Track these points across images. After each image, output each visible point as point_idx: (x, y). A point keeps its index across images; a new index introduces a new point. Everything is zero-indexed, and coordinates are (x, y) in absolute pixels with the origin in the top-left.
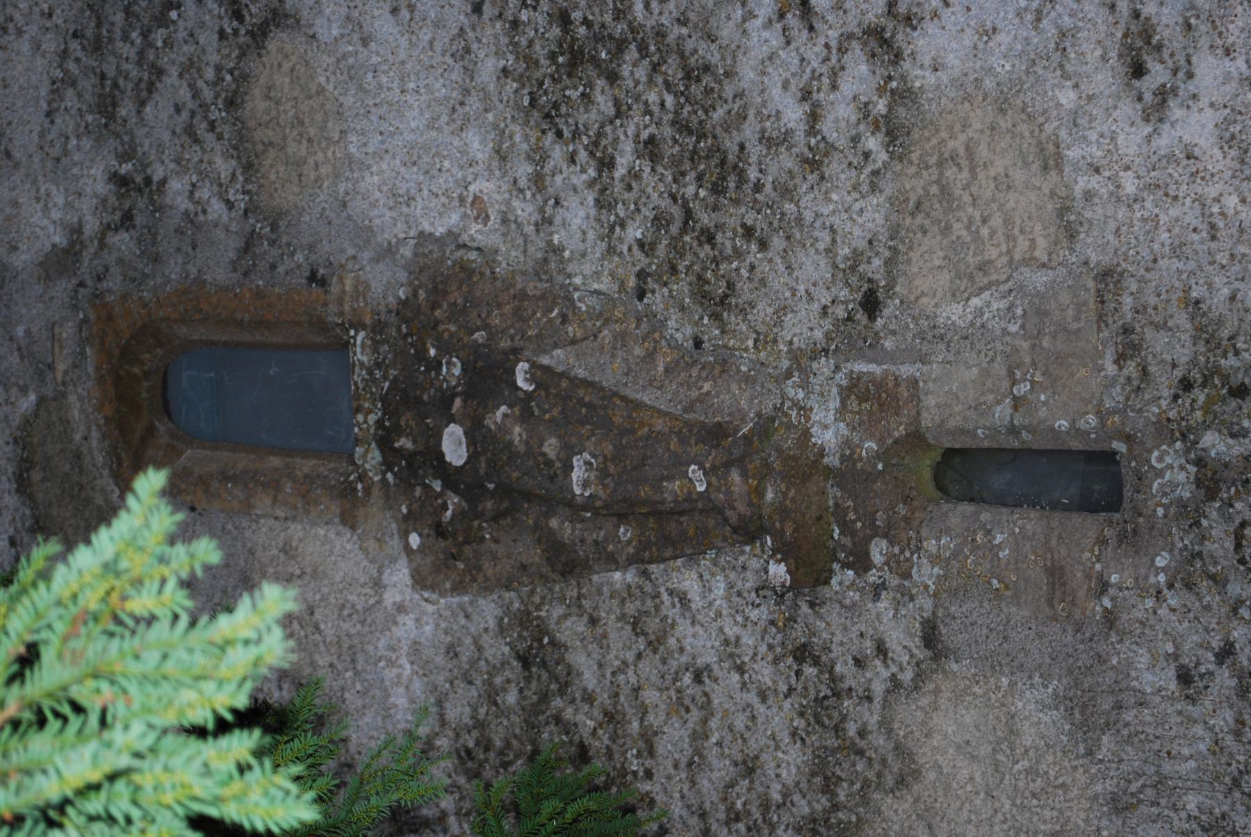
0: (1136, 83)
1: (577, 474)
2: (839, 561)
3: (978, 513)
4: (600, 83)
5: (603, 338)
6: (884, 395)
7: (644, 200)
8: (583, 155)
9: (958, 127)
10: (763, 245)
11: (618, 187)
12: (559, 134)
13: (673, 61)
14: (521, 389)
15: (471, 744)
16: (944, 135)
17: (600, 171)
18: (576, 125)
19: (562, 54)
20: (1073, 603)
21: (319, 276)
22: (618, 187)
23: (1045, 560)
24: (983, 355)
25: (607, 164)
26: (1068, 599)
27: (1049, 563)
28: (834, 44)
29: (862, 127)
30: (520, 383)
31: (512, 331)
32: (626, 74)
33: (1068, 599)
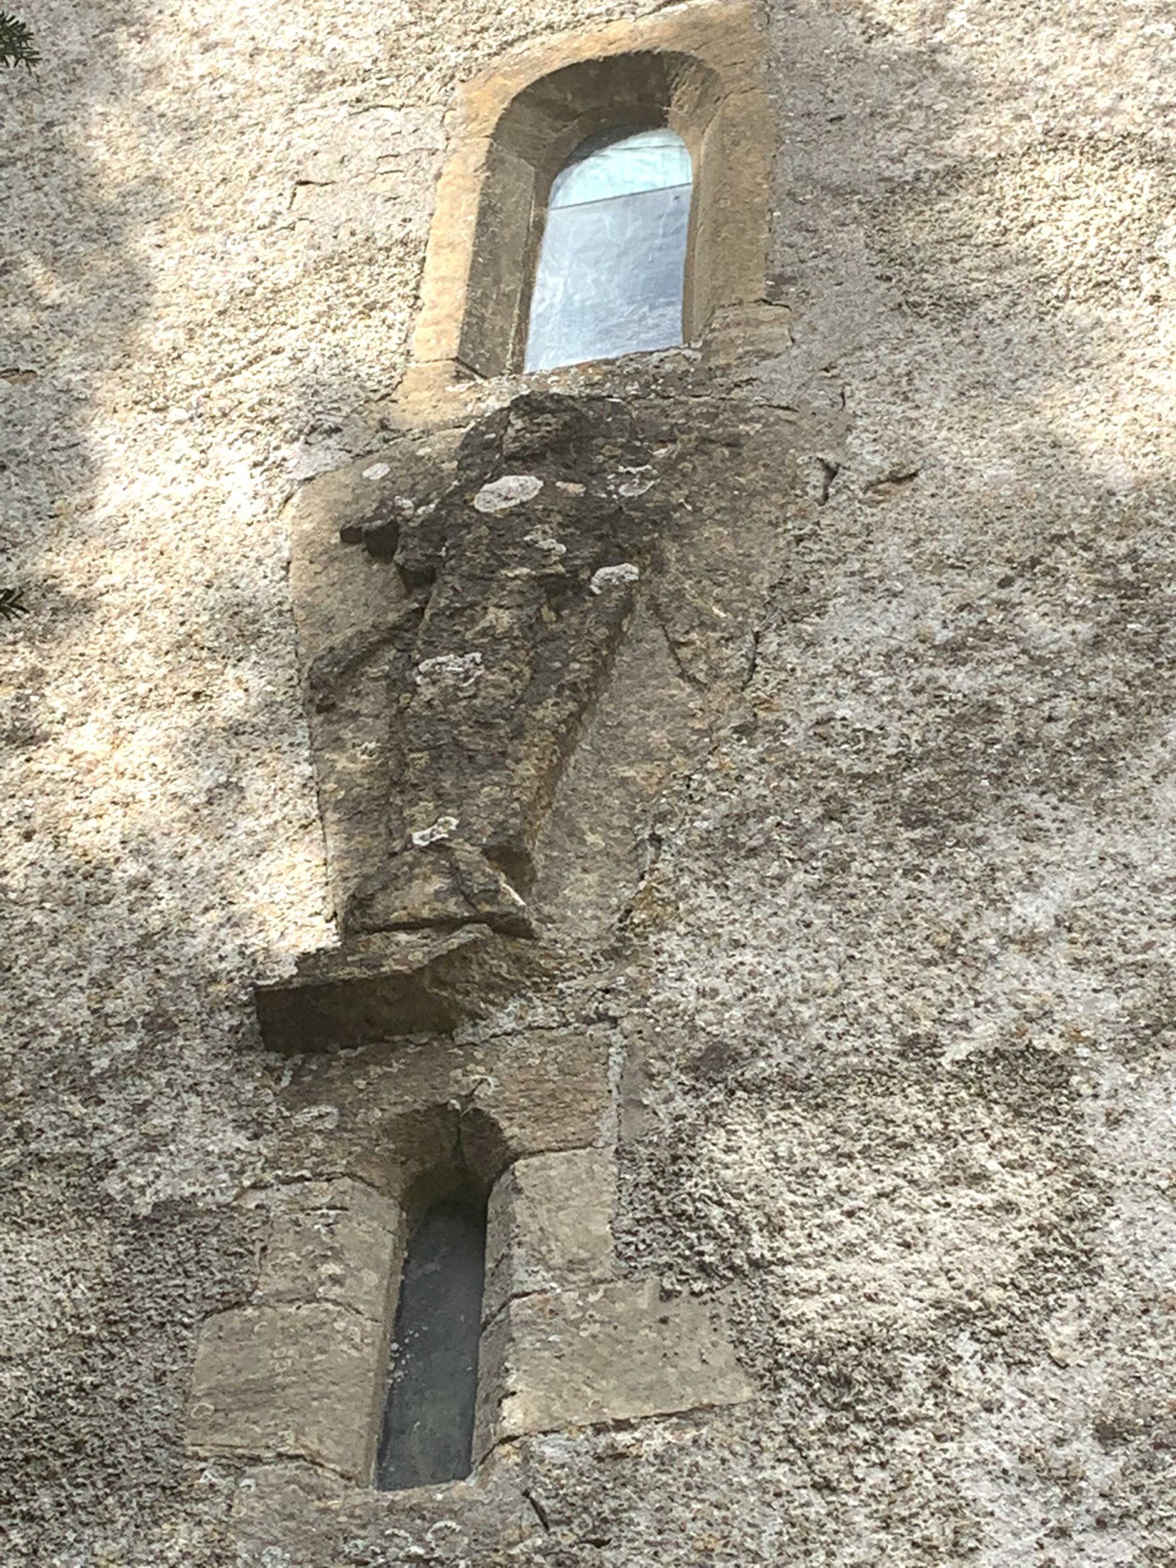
0: (1086, 1432)
1: (452, 663)
2: (304, 1061)
3: (377, 1265)
4: (1085, 629)
5: (678, 687)
6: (568, 1098)
7: (898, 712)
8: (969, 619)
9: (1009, 1155)
10: (818, 892)
11: (921, 674)
12: (1006, 583)
13: (1116, 725)
14: (593, 574)
15: (339, 766)
16: (996, 1136)
17: (944, 647)
18: (1021, 604)
19: (1135, 570)
20: (215, 1427)
21: (784, 288)
22: (921, 674)
23: (286, 1374)
24: (630, 1238)
25: (954, 653)
26: (220, 1418)
27: (279, 1379)
28: (1151, 955)
29: (1011, 1012)
30: (602, 572)
31: (692, 559)
32: (1101, 661)
33: (220, 1418)
